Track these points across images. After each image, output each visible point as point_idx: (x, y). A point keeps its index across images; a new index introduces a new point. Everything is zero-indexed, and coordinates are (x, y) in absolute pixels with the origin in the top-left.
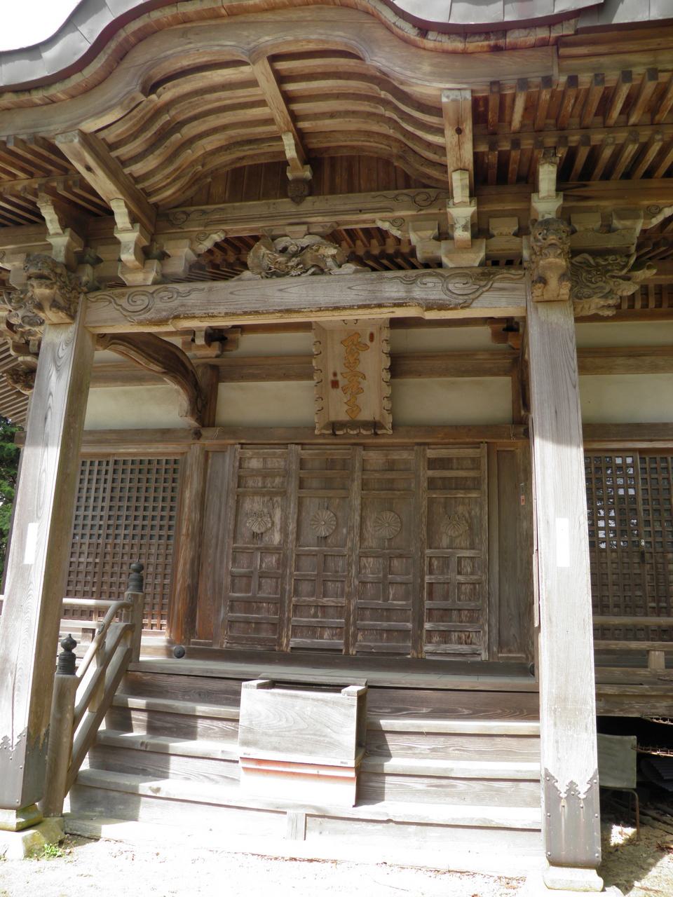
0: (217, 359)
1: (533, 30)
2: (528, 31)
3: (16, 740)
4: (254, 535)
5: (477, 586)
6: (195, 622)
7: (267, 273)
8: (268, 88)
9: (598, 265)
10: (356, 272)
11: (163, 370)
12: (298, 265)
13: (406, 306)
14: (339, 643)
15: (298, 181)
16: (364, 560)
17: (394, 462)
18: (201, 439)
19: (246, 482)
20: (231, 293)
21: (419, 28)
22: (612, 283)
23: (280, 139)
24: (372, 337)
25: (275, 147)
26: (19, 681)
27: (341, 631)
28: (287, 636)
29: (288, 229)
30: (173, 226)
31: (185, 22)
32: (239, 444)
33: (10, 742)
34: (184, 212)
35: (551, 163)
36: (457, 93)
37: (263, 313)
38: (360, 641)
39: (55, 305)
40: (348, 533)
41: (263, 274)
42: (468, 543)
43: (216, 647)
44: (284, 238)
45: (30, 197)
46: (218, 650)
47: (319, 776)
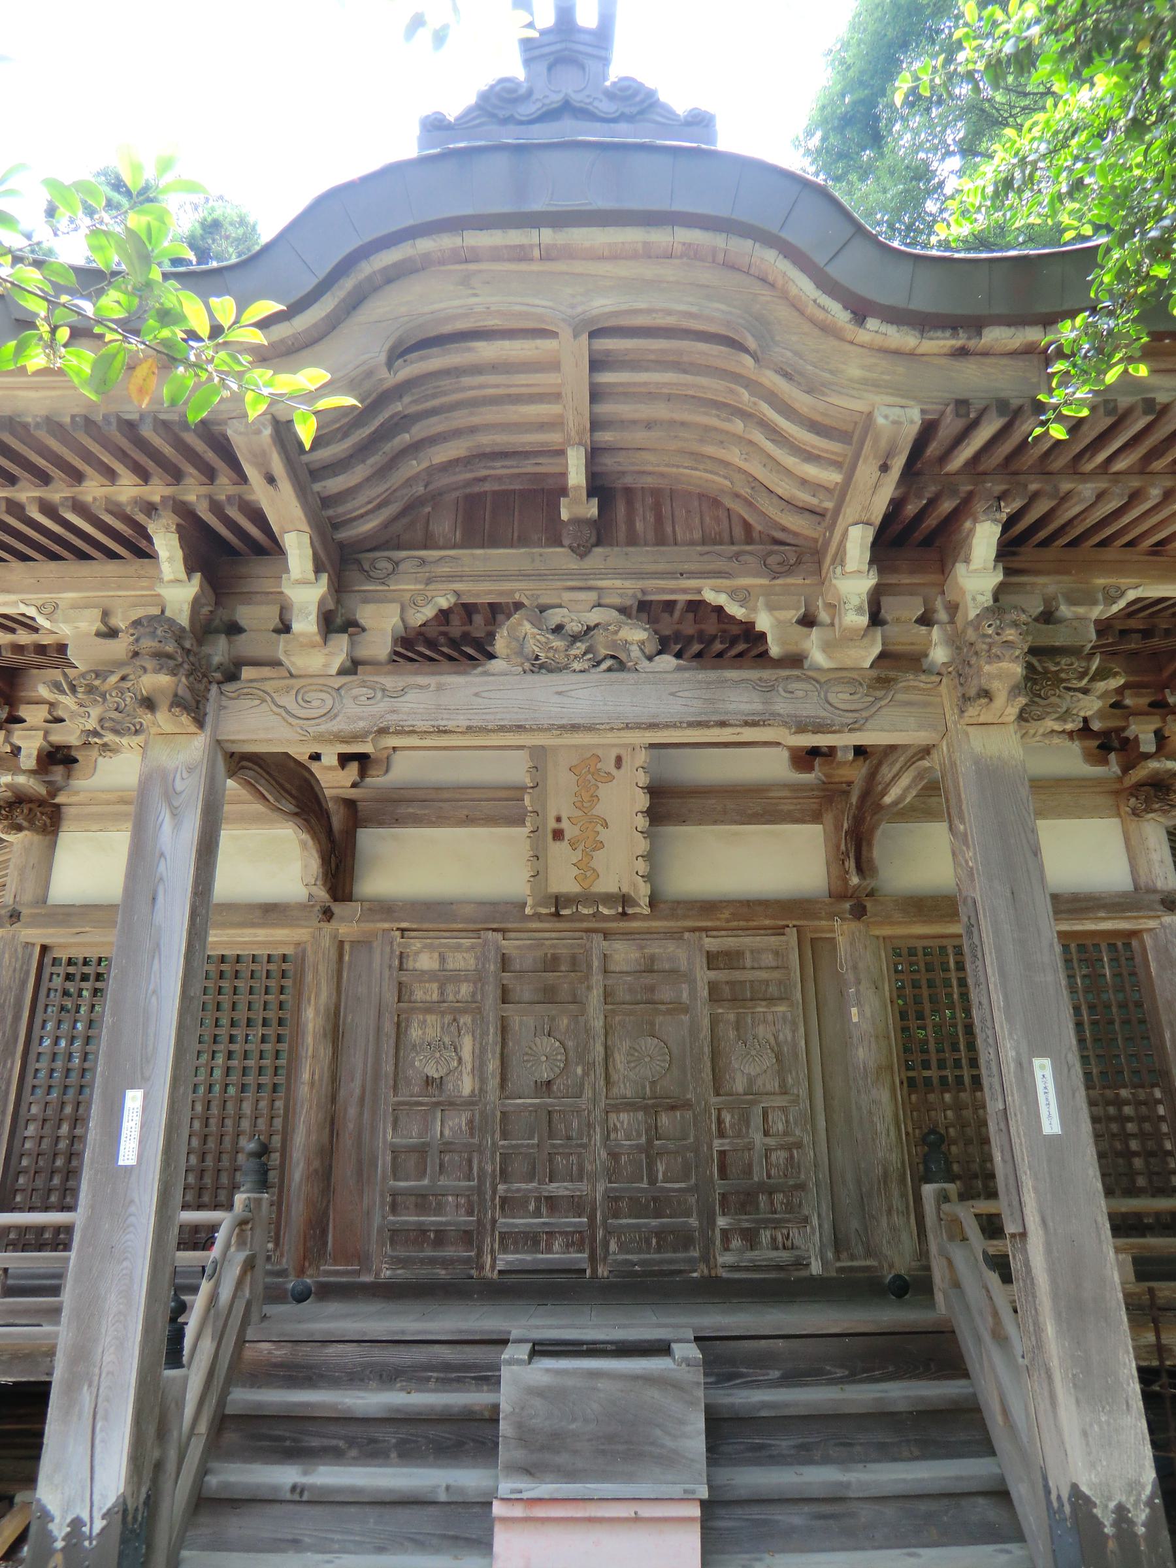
0: (354, 790)
1: (1021, 329)
2: (1013, 330)
3: (99, 1524)
4: (428, 1081)
5: (795, 1152)
6: (327, 1236)
7: (533, 665)
8: (574, 377)
9: (1046, 671)
10: (679, 669)
11: (297, 810)
12: (585, 654)
13: (764, 725)
14: (579, 1258)
15: (577, 522)
16: (613, 1117)
17: (652, 958)
18: (333, 922)
19: (411, 993)
20: (476, 695)
21: (852, 312)
22: (1068, 698)
23: (561, 453)
24: (619, 761)
25: (547, 466)
26: (107, 1400)
27: (577, 1240)
28: (492, 1251)
29: (567, 596)
30: (370, 578)
31: (466, 261)
32: (398, 929)
33: (86, 1529)
34: (389, 559)
35: (995, 521)
36: (898, 410)
37: (532, 730)
38: (614, 1253)
39: (177, 702)
40: (586, 1074)
41: (527, 666)
42: (777, 1085)
43: (367, 1278)
44: (557, 610)
45: (141, 518)
46: (372, 1283)
47: (637, 1519)
